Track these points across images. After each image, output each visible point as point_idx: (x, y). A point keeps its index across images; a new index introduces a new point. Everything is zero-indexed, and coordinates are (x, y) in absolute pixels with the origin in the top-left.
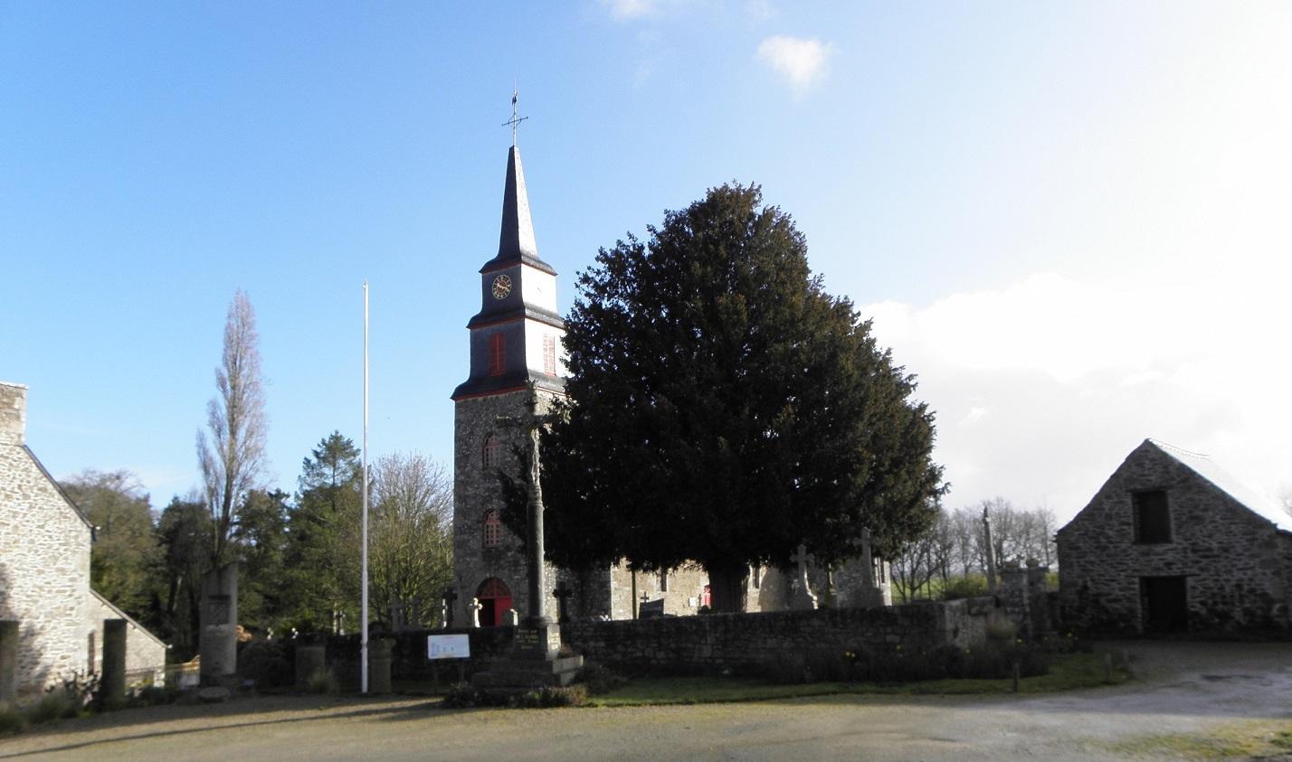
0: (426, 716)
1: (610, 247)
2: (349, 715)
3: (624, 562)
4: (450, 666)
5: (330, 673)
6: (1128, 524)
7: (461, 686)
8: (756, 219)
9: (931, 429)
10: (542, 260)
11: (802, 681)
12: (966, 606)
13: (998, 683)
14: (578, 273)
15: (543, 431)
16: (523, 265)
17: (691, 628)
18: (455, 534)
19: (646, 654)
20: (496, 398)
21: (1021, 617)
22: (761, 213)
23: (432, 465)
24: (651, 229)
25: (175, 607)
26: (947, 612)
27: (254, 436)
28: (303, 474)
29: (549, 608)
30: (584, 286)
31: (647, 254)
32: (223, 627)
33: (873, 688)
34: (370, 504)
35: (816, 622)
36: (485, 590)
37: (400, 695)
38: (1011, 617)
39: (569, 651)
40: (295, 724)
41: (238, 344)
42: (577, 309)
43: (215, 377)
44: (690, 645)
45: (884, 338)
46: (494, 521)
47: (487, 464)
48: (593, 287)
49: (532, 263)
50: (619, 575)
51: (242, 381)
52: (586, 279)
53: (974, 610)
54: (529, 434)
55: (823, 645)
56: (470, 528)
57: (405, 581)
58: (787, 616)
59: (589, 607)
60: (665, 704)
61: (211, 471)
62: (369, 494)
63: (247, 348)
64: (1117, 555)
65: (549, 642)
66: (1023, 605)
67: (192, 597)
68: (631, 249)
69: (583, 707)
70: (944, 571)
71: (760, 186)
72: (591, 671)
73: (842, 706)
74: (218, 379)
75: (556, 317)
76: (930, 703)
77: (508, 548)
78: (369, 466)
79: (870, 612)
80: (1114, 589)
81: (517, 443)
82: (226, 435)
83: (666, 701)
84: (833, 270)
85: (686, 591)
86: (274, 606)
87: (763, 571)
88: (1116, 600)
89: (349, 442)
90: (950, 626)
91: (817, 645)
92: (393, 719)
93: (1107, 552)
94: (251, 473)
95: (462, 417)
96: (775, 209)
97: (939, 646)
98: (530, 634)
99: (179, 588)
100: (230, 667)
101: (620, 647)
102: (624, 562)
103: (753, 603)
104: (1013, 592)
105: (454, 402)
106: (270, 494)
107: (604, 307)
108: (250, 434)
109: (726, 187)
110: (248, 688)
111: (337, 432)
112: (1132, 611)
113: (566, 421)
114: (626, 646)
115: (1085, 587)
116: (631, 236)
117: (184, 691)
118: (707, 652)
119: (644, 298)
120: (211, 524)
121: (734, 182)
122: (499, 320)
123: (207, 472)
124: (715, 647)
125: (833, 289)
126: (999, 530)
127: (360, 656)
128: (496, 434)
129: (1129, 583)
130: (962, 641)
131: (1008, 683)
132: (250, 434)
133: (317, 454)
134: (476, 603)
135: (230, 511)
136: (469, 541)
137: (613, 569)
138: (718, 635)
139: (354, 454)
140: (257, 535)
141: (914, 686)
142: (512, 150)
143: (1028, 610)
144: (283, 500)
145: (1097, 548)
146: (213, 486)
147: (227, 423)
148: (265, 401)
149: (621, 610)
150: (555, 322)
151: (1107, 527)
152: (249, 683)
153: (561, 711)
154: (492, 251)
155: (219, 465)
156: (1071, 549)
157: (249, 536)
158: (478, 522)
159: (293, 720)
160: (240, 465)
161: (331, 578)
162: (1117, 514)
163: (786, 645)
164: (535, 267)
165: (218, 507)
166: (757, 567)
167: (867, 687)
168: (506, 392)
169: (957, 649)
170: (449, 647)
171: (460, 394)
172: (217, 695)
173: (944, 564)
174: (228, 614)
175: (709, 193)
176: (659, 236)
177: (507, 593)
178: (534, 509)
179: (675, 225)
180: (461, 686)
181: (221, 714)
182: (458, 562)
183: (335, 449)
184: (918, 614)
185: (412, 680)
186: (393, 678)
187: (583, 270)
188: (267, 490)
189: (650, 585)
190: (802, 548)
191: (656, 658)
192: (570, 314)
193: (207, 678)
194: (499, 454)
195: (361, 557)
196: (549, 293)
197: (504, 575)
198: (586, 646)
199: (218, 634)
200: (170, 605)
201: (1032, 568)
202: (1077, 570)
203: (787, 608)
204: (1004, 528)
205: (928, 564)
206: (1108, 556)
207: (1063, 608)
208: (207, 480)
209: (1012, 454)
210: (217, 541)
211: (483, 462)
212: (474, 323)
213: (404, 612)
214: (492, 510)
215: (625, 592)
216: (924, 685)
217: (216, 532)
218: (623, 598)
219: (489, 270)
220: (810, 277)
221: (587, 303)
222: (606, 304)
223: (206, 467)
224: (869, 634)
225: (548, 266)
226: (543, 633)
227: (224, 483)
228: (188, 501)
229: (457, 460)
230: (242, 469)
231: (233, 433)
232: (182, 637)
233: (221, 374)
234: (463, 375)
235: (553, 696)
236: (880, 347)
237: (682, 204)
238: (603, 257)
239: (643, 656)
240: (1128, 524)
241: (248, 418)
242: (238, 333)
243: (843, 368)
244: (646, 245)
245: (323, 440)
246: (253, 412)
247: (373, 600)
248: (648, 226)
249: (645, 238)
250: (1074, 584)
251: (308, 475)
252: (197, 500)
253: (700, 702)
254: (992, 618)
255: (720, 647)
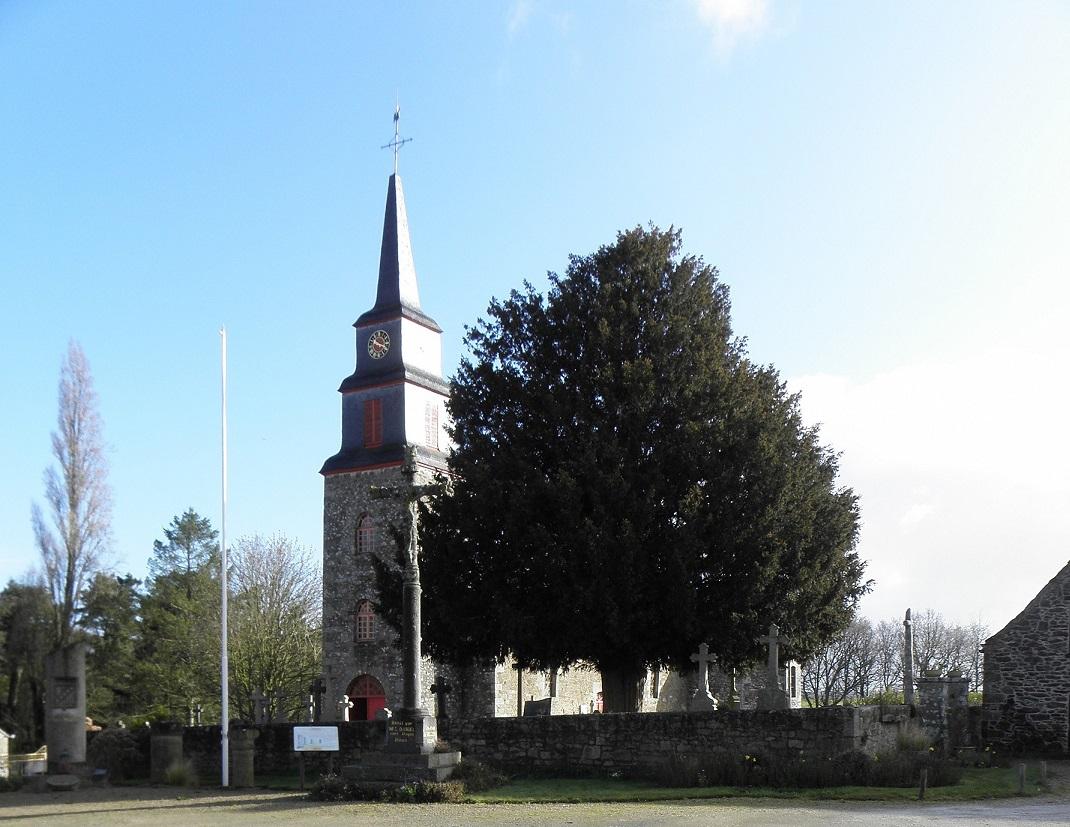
0: (292, 807)
1: (504, 297)
2: (209, 805)
3: (510, 660)
4: (318, 760)
5: (189, 764)
6: (1065, 635)
7: (329, 778)
8: (674, 271)
9: (856, 526)
10: (425, 314)
11: (696, 784)
12: (877, 713)
13: (904, 792)
14: (466, 327)
15: (421, 506)
16: (403, 319)
17: (579, 728)
18: (324, 626)
19: (529, 754)
20: (372, 473)
21: (937, 730)
22: (679, 264)
23: (299, 550)
24: (553, 277)
25: (15, 702)
26: (856, 717)
27: (97, 511)
28: (154, 556)
29: (426, 702)
30: (473, 342)
31: (545, 308)
32: (72, 712)
33: (771, 793)
34: (230, 593)
35: (714, 724)
36: (356, 689)
37: (264, 789)
38: (925, 729)
39: (445, 745)
40: (151, 811)
41: (76, 403)
42: (463, 371)
43: (51, 444)
44: (578, 746)
45: (809, 415)
46: (367, 614)
47: (361, 549)
48: (483, 345)
49: (414, 316)
50: (504, 673)
51: (81, 447)
52: (475, 335)
53: (885, 718)
54: (406, 506)
55: (722, 749)
56: (341, 619)
57: (268, 678)
58: (684, 717)
59: (470, 711)
60: (547, 802)
61: (50, 549)
62: (229, 579)
63: (85, 410)
64: (1048, 668)
65: (424, 736)
66: (941, 717)
67: (34, 688)
68: (528, 301)
69: (460, 803)
70: (862, 689)
71: (680, 230)
72: (469, 768)
73: (735, 808)
74: (54, 444)
75: (440, 382)
76: (829, 808)
77: (382, 643)
78: (229, 551)
79: (775, 717)
80: (1042, 705)
81: (394, 524)
82: (66, 509)
83: (549, 799)
84: (761, 333)
85: (578, 691)
86: (124, 702)
87: (664, 675)
88: (1041, 717)
89: (205, 522)
90: (858, 733)
91: (715, 749)
92: (256, 810)
93: (1038, 664)
94: (96, 552)
95: (332, 494)
96: (696, 259)
97: (844, 753)
98: (404, 726)
99: (19, 681)
100: (80, 754)
101: (501, 746)
102: (510, 660)
103: (649, 704)
104: (931, 703)
105: (323, 477)
106: (120, 579)
107: (494, 369)
108: (92, 507)
109: (639, 230)
110: (100, 777)
111: (191, 510)
112: (1058, 728)
113: (448, 493)
114: (509, 746)
115: (1011, 702)
116: (528, 285)
117: (33, 777)
118: (595, 753)
119: (542, 362)
120: (53, 610)
121: (650, 223)
122: (375, 384)
123: (45, 551)
124: (604, 748)
125: (757, 356)
126: (927, 645)
127: (220, 748)
128: (371, 516)
129: (1058, 699)
130: (871, 749)
131: (914, 792)
132: (92, 507)
133: (169, 534)
134: (346, 701)
135: (74, 597)
136: (339, 633)
137: (499, 669)
138: (608, 736)
139: (212, 537)
140: (105, 624)
141: (814, 792)
142: (392, 179)
143: (945, 722)
144: (134, 587)
145: (1026, 660)
146: (53, 567)
147: (67, 495)
148: (108, 471)
149: (505, 707)
150: (439, 388)
151: (1041, 637)
152: (102, 772)
153: (436, 805)
154: (368, 302)
155: (60, 543)
156: (999, 660)
157: (96, 624)
158: (350, 613)
159: (150, 808)
160: (82, 542)
161: (186, 671)
162: (1053, 622)
163: (681, 748)
164: (418, 323)
165: (59, 589)
166: (656, 670)
167: (763, 791)
168: (381, 467)
169: (863, 756)
170: (316, 739)
171: (331, 467)
172: (66, 784)
173: (863, 681)
174: (75, 698)
175: (621, 237)
176: (561, 286)
177: (381, 692)
178: (410, 591)
179: (580, 274)
180: (329, 778)
181: (71, 802)
182: (327, 656)
183: (189, 529)
184: (827, 720)
185: (275, 768)
186: (257, 773)
187: (473, 324)
188: (117, 574)
189: (537, 685)
190: (704, 647)
191: (541, 759)
192: (457, 375)
193: (53, 765)
194: (374, 537)
195: (220, 650)
196: (433, 354)
197: (377, 673)
198: (465, 744)
199: (66, 719)
200: (11, 699)
201: (954, 680)
202: (1004, 683)
203: (684, 708)
204: (932, 643)
205: (845, 681)
206: (1038, 668)
207: (984, 724)
208: (46, 558)
209: (939, 561)
210: (60, 626)
211: (356, 547)
212: (347, 386)
213: (268, 710)
214: (365, 601)
215: (510, 689)
216: (826, 791)
217: (59, 618)
218: (508, 702)
219: (365, 322)
220: (731, 340)
221: (475, 363)
222: (497, 365)
223: (44, 544)
224: (770, 739)
225: (432, 321)
226: (418, 725)
227: (65, 563)
228: (26, 583)
229: (327, 544)
230: (86, 548)
231: (74, 505)
232: (25, 732)
233: (57, 438)
234: (334, 447)
235: (428, 791)
236: (807, 423)
237: (588, 249)
238: (494, 310)
239: (527, 756)
240: (1065, 635)
241: (90, 490)
242: (74, 391)
243: (763, 450)
244: (545, 297)
245: (176, 518)
246: (96, 483)
247: (234, 697)
248: (549, 273)
249: (544, 289)
250: (999, 699)
251: (160, 557)
252: (35, 582)
253: (585, 801)
254: (904, 728)
255: (610, 748)
